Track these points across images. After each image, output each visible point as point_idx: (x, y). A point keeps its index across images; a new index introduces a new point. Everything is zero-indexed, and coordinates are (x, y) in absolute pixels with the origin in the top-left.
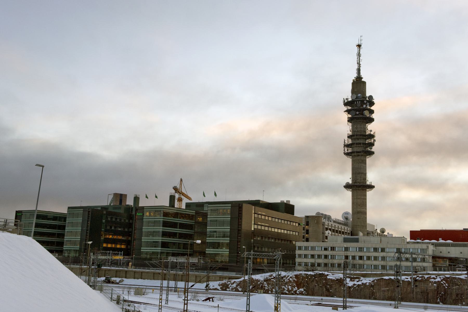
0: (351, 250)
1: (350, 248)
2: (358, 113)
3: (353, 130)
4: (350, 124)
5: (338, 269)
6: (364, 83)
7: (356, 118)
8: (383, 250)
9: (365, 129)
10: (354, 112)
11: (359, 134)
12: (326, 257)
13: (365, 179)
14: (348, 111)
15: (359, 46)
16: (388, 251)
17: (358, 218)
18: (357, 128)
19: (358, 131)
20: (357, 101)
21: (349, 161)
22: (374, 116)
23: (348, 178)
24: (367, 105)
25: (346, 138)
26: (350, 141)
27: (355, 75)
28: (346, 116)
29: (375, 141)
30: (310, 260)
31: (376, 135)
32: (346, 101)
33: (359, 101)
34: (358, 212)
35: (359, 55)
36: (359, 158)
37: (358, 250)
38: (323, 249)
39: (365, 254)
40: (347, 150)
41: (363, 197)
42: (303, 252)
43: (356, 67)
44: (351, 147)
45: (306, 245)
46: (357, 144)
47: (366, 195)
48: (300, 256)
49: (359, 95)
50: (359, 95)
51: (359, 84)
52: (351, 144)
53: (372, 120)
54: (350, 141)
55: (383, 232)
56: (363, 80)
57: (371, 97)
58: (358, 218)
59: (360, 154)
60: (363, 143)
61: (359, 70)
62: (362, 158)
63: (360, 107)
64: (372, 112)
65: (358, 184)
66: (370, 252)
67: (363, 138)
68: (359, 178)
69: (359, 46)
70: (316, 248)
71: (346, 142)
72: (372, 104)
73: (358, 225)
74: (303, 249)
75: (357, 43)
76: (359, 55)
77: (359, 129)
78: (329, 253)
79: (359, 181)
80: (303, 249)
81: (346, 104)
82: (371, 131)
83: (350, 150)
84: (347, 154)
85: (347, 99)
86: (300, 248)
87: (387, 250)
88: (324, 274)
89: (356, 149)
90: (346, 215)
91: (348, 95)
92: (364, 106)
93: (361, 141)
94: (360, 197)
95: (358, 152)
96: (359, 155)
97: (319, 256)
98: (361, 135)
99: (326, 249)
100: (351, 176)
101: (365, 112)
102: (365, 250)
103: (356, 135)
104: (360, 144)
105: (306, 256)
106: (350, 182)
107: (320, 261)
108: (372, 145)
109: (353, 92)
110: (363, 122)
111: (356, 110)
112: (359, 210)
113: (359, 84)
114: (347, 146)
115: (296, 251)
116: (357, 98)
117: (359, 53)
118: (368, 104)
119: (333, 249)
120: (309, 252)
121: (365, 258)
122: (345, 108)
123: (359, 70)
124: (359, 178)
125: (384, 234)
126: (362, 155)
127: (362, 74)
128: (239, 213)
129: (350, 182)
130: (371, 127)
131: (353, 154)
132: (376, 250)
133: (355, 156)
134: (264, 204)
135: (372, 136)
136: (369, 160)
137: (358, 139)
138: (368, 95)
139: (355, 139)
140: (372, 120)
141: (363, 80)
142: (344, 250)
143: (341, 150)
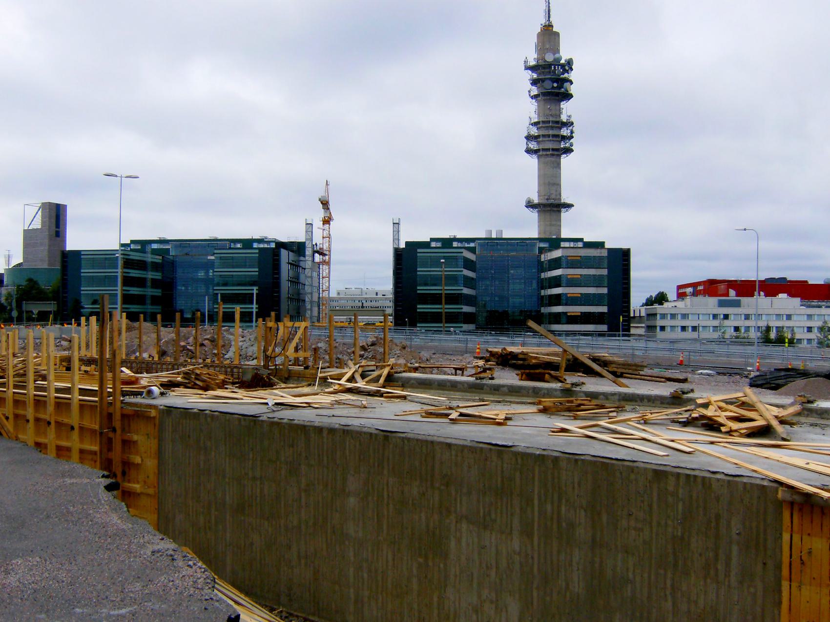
6: (557, 34)
26: (534, 131)
27: (543, 21)
43: (544, 6)
47: (559, 165)
51: (548, 36)
53: (568, 96)
57: (570, 63)
63: (552, 81)
83: (533, 145)
84: (529, 151)
93: (555, 132)
113: (548, 36)
130: (567, 109)
140: (568, 96)
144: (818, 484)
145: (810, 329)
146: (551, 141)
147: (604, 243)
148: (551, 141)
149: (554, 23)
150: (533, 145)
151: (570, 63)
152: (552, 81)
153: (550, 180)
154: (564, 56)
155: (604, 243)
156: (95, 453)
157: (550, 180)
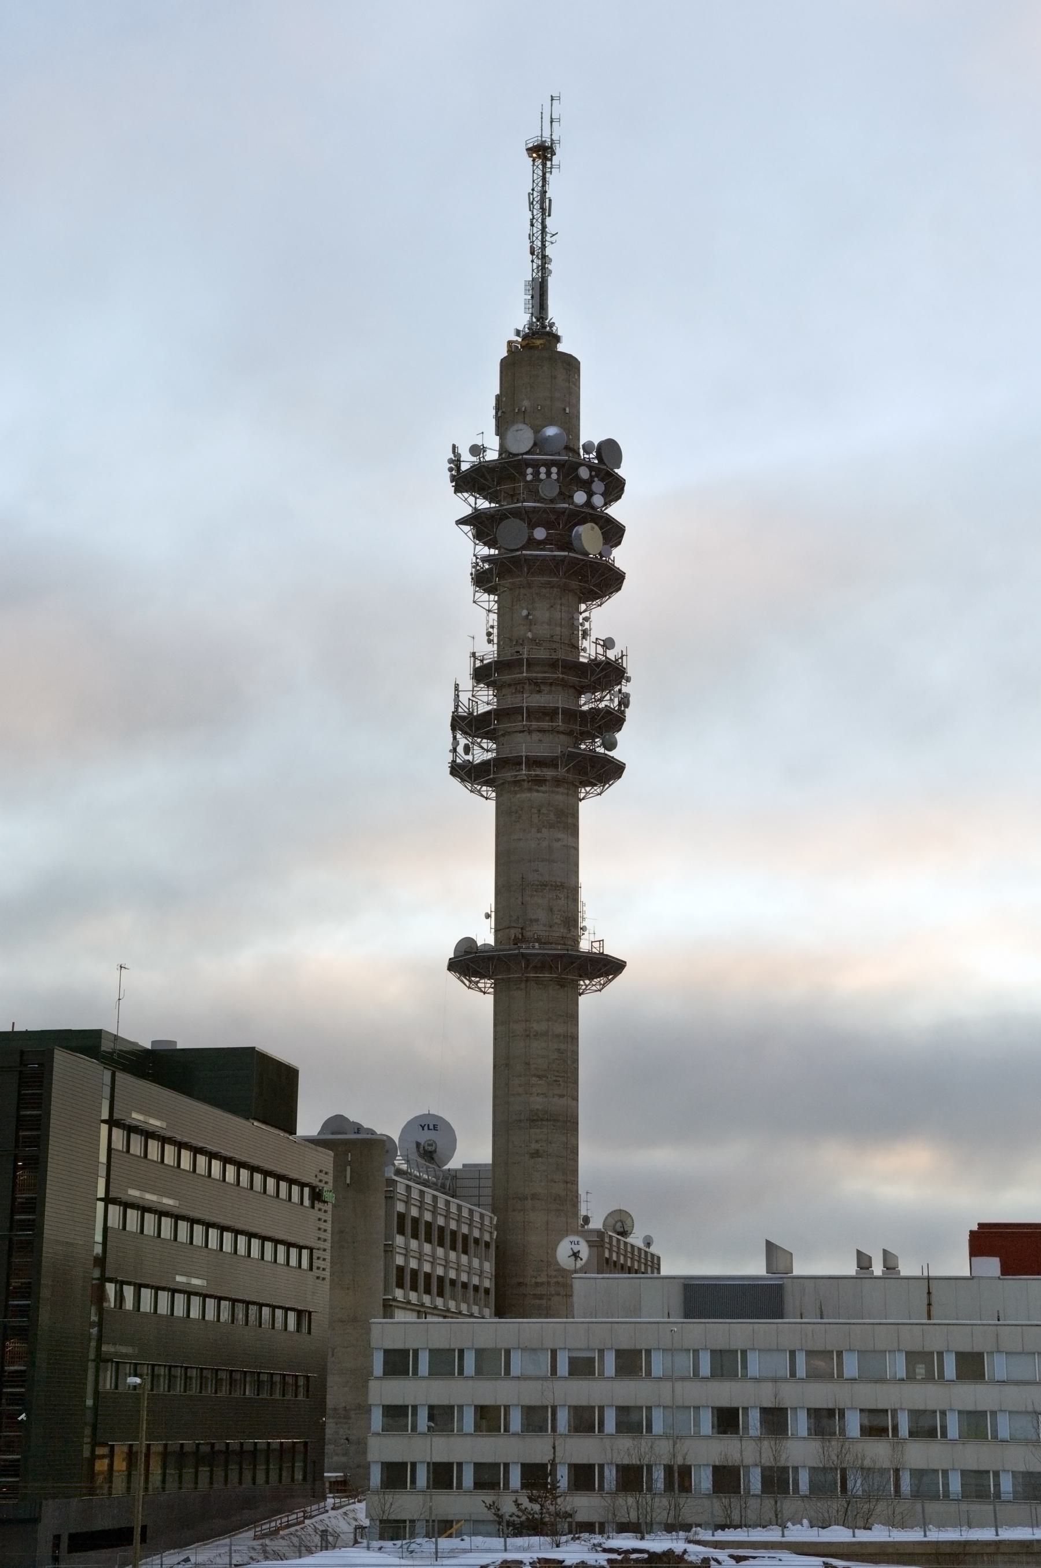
0: (754, 1367)
1: (753, 1358)
2: (540, 533)
3: (506, 631)
4: (490, 601)
5: (717, 1507)
6: (571, 365)
7: (530, 561)
8: (971, 1366)
9: (572, 634)
10: (513, 531)
11: (543, 654)
12: (585, 1421)
13: (571, 921)
14: (480, 525)
15: (542, 152)
16: (1001, 1373)
17: (536, 1154)
18: (529, 621)
19: (535, 641)
20: (536, 465)
21: (480, 810)
22: (620, 557)
23: (472, 914)
24: (590, 494)
25: (467, 682)
26: (485, 700)
27: (522, 319)
28: (466, 551)
29: (625, 701)
30: (513, 1450)
31: (631, 668)
32: (468, 462)
33: (548, 465)
34: (535, 1119)
35: (541, 205)
36: (537, 796)
37: (801, 1371)
38: (563, 1368)
39: (854, 1398)
40: (467, 750)
41: (559, 1029)
42: (419, 1391)
43: (525, 270)
44: (490, 736)
45: (440, 1342)
46: (534, 714)
47: (572, 1017)
48: (397, 1415)
49: (551, 431)
50: (551, 431)
51: (538, 371)
52: (498, 714)
53: (609, 580)
54: (485, 700)
55: (624, 1233)
56: (561, 348)
57: (610, 451)
58: (536, 1154)
59: (549, 773)
60: (565, 711)
61: (539, 293)
62: (559, 798)
63: (544, 510)
64: (614, 533)
65: (537, 949)
66: (882, 1380)
67: (564, 684)
68: (541, 915)
69: (542, 152)
70: (516, 1358)
71: (464, 697)
72: (615, 488)
73: (535, 1197)
74: (424, 1368)
75: (532, 135)
76: (541, 205)
77: (543, 631)
78: (607, 1391)
79: (538, 930)
80: (424, 1368)
81: (465, 481)
82: (608, 644)
83: (483, 752)
84: (465, 772)
85: (476, 450)
86: (399, 1363)
87: (998, 1367)
88: (680, 1558)
89: (526, 745)
90: (424, 1137)
91: (479, 432)
92: (580, 497)
93: (557, 700)
94: (542, 1027)
95: (535, 762)
96: (539, 781)
97: (537, 1419)
98: (553, 664)
99: (582, 1368)
100: (488, 900)
101: (581, 529)
102: (851, 1366)
103: (531, 664)
104: (550, 713)
105: (442, 1417)
106: (485, 935)
107: (584, 1449)
108: (614, 720)
109: (506, 414)
110: (565, 589)
111: (532, 519)
112: (537, 1102)
113: (538, 371)
114: (465, 723)
115: (373, 1385)
116: (538, 444)
117: (544, 193)
118: (598, 486)
119: (630, 1363)
120: (464, 1392)
121: (853, 1424)
122: (465, 505)
123: (539, 293)
124: (541, 915)
125: (630, 1240)
126: (558, 782)
127: (560, 314)
128: (21, 1122)
129: (485, 935)
130: (604, 622)
131: (508, 775)
132: (922, 1363)
133: (517, 783)
134: (132, 1053)
135: (610, 673)
136: (594, 810)
137: (537, 686)
138: (591, 431)
139: (518, 686)
140: (609, 580)
141: (561, 348)
142: (705, 1369)
143: (440, 744)
144: (751, 1562)
145: (727, 1420)
146: (544, 733)
147: (971, 1232)
148: (544, 733)
149: (560, 329)
150: (483, 752)
151: (610, 451)
152: (544, 510)
153: (537, 878)
154: (591, 431)
155: (971, 1232)
156: (244, 1394)
157: (537, 878)
